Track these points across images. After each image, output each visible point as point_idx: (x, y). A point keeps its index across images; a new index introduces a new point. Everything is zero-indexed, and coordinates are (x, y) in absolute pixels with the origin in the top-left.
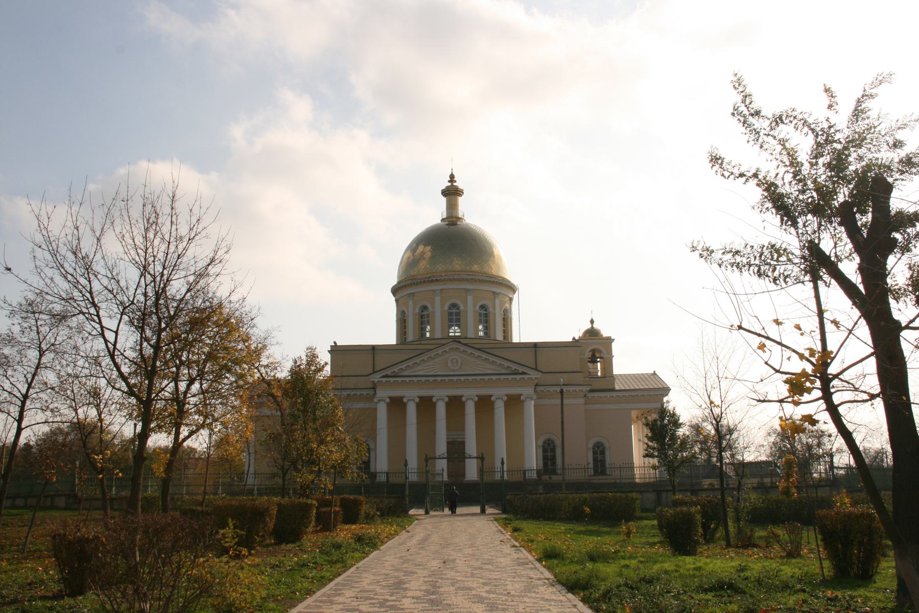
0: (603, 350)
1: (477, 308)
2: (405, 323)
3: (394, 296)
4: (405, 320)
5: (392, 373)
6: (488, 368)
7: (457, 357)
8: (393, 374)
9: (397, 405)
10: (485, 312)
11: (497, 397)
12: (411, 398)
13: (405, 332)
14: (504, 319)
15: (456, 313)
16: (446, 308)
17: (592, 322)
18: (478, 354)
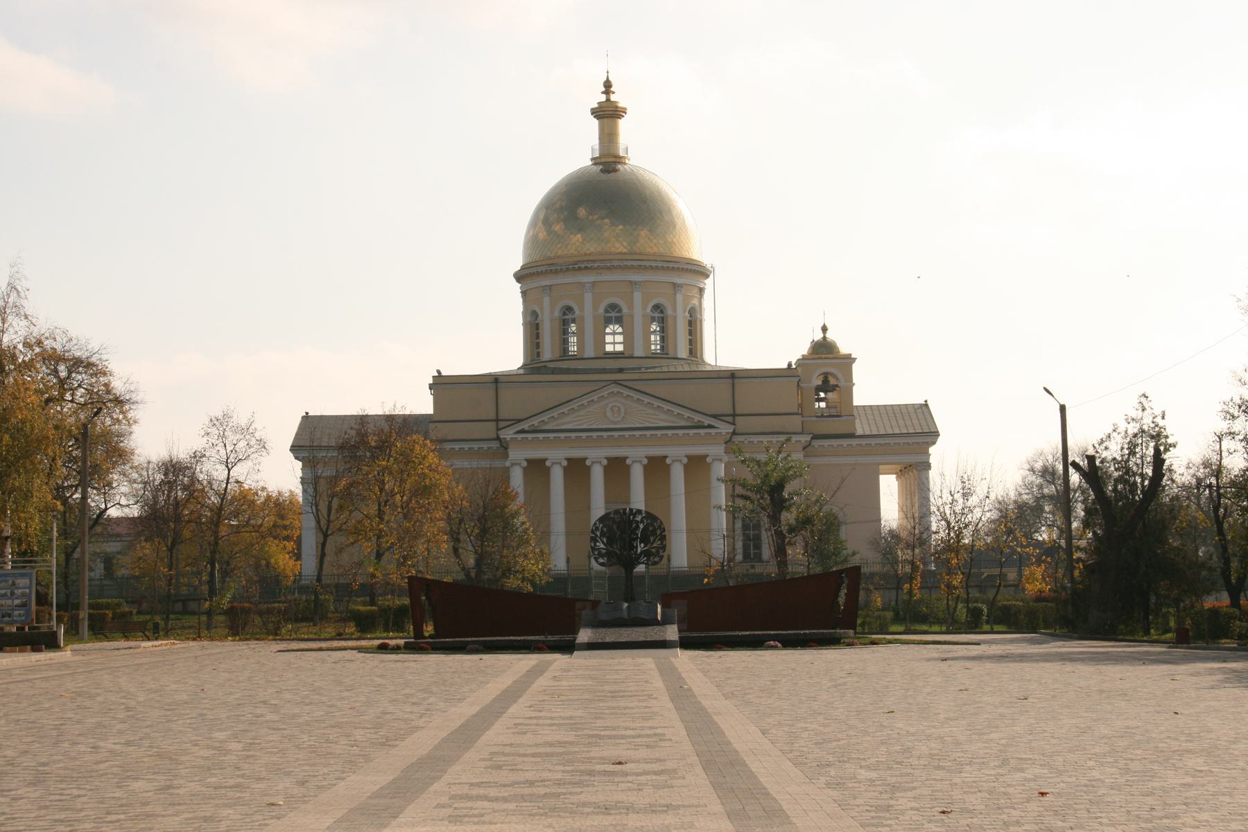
0: (840, 376)
1: (649, 310)
2: (537, 328)
4: (537, 325)
5: (529, 427)
7: (618, 405)
8: (532, 428)
9: (537, 469)
10: (617, 315)
14: (690, 323)
16: (601, 310)
17: (824, 329)
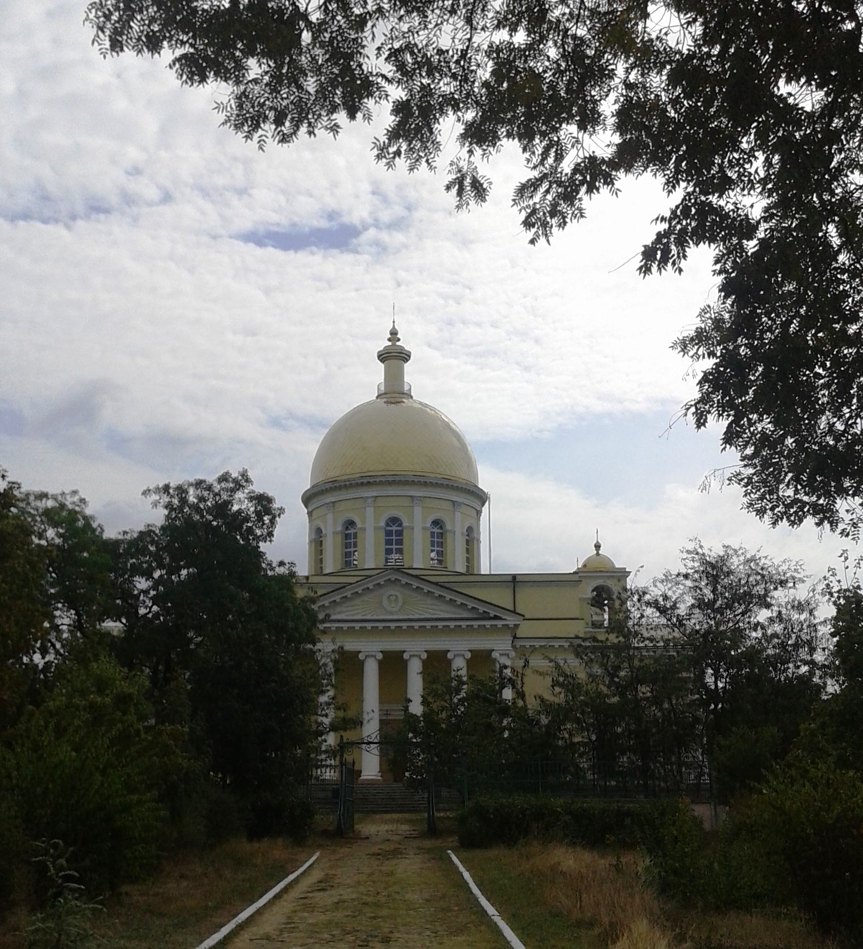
1: (428, 525)
3: (306, 506)
6: (443, 611)
7: (393, 593)
11: (367, 654)
12: (371, 654)
13: (321, 559)
15: (396, 531)
16: (383, 524)
17: (598, 547)
18: (439, 593)
